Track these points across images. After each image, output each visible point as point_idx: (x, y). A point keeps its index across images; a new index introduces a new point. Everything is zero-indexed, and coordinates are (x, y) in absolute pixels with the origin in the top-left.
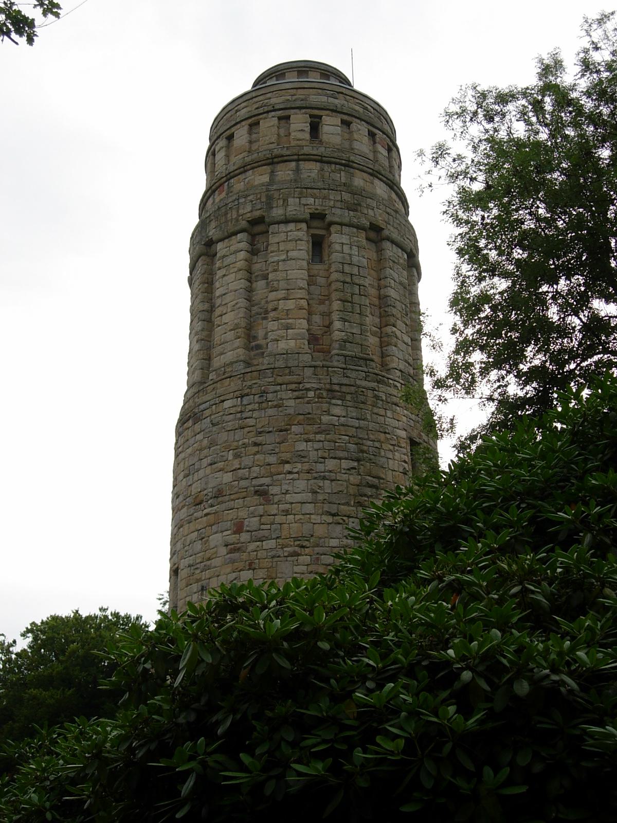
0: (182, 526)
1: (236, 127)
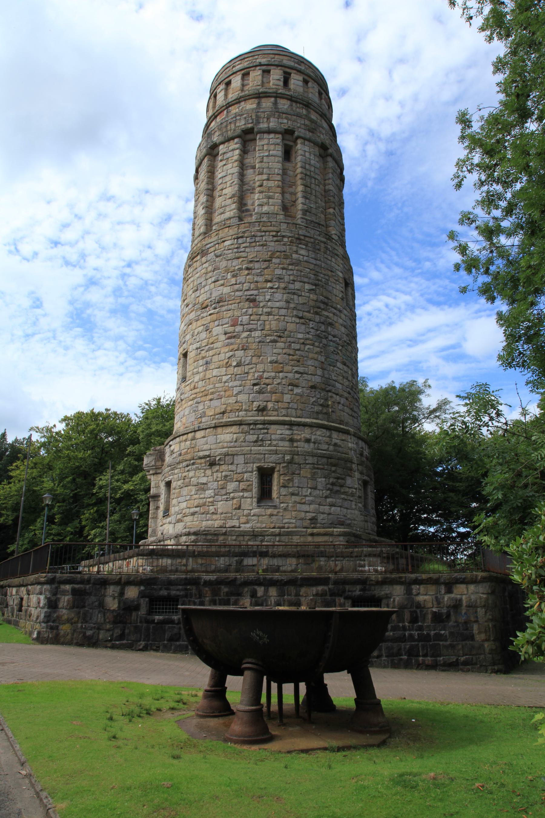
0: (191, 324)
1: (233, 76)
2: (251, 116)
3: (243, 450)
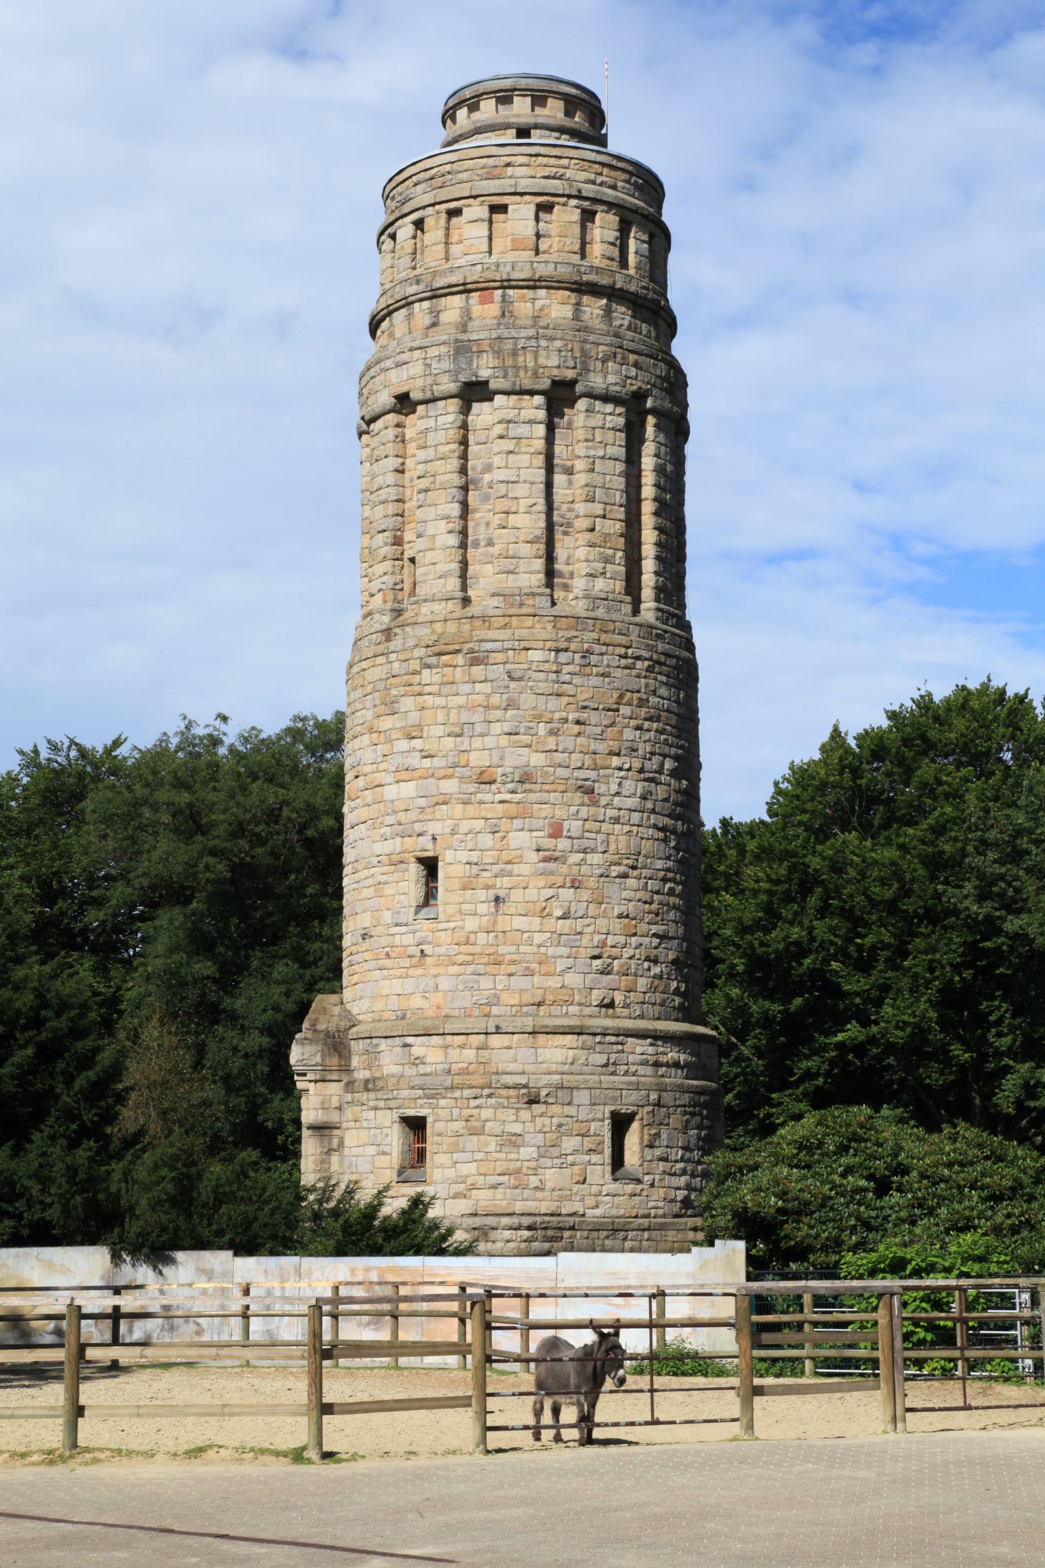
2: (572, 350)
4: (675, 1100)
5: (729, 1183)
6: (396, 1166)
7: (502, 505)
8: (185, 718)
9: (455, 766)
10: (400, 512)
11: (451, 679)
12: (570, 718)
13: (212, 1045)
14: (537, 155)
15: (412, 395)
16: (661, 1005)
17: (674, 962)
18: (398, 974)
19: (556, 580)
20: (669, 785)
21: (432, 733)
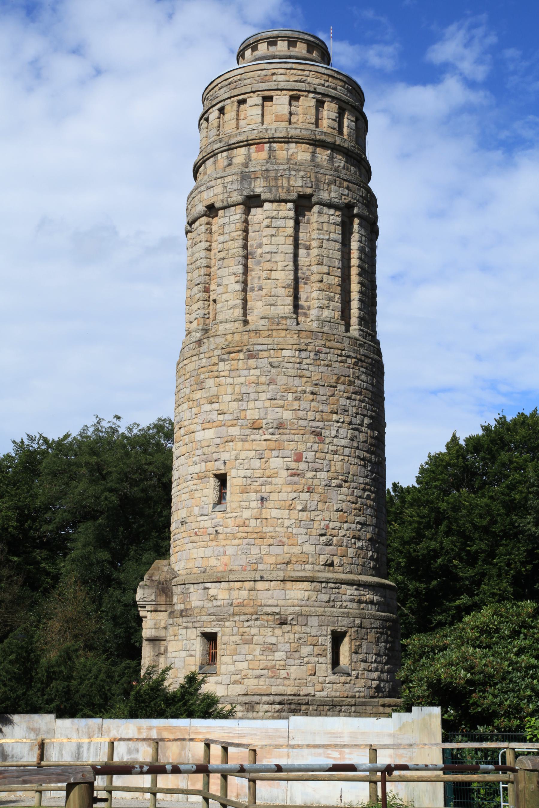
2: (310, 177)
3: (317, 611)
4: (371, 624)
5: (424, 660)
6: (198, 664)
7: (268, 266)
8: (97, 417)
9: (238, 419)
10: (208, 273)
11: (236, 368)
12: (308, 390)
13: (106, 598)
14: (290, 69)
15: (215, 205)
16: (362, 566)
17: (370, 540)
18: (202, 545)
19: (300, 311)
20: (367, 433)
21: (224, 400)
